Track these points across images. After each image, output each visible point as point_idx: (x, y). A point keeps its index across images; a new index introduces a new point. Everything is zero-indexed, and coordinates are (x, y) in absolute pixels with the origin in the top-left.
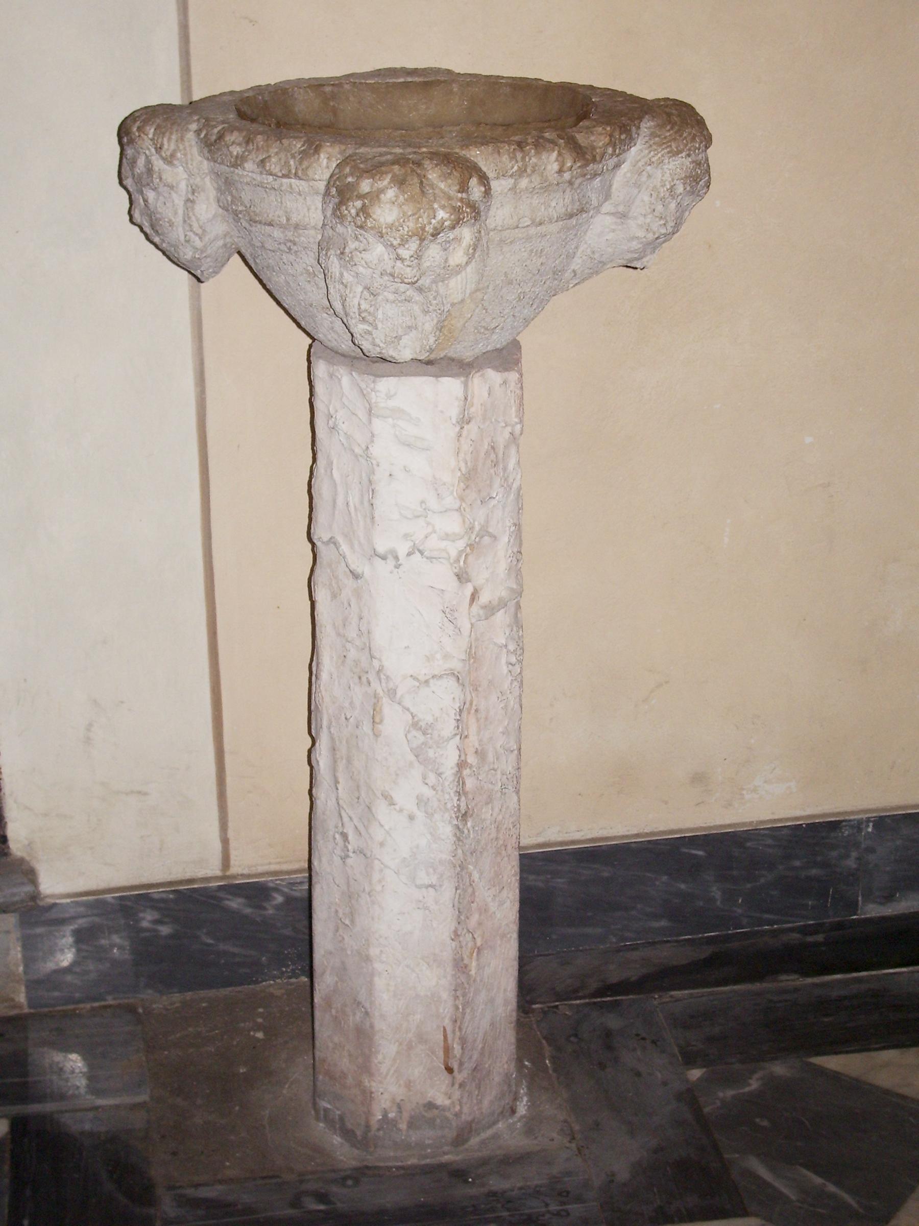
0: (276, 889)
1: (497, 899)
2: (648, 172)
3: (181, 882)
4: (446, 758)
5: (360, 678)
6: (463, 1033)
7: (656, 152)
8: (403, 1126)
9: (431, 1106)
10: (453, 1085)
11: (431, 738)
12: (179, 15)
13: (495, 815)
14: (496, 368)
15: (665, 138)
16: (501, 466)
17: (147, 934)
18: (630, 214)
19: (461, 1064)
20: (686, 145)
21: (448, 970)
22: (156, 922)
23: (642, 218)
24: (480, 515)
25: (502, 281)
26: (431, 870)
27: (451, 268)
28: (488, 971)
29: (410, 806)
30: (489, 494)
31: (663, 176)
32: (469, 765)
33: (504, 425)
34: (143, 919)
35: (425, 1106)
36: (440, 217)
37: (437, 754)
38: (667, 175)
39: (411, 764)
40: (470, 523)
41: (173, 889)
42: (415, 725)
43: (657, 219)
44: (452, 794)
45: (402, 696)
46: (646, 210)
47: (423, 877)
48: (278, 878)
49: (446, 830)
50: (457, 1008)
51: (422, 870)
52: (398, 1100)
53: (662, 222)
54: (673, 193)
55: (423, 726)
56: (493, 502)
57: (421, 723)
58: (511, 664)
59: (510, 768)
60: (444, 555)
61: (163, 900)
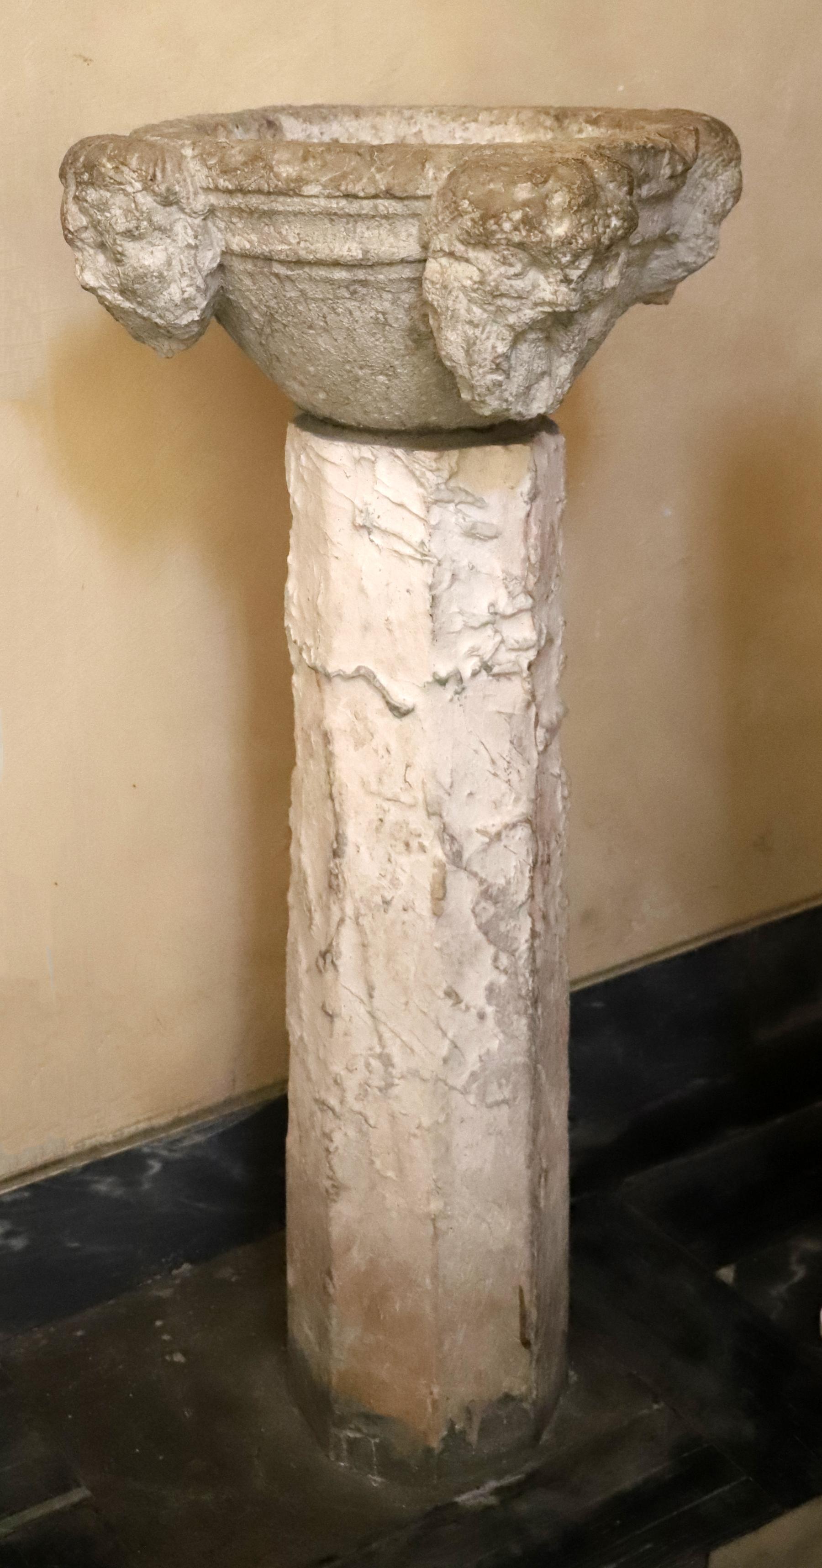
0: (153, 1155)
3: (32, 1171)
8: (473, 1437)
9: (507, 1398)
26: (504, 1081)
38: (721, 188)
41: (28, 1183)
42: (486, 894)
44: (527, 975)
45: (470, 859)
47: (496, 1094)
48: (154, 1138)
55: (494, 893)
60: (516, 669)
61: (14, 1203)
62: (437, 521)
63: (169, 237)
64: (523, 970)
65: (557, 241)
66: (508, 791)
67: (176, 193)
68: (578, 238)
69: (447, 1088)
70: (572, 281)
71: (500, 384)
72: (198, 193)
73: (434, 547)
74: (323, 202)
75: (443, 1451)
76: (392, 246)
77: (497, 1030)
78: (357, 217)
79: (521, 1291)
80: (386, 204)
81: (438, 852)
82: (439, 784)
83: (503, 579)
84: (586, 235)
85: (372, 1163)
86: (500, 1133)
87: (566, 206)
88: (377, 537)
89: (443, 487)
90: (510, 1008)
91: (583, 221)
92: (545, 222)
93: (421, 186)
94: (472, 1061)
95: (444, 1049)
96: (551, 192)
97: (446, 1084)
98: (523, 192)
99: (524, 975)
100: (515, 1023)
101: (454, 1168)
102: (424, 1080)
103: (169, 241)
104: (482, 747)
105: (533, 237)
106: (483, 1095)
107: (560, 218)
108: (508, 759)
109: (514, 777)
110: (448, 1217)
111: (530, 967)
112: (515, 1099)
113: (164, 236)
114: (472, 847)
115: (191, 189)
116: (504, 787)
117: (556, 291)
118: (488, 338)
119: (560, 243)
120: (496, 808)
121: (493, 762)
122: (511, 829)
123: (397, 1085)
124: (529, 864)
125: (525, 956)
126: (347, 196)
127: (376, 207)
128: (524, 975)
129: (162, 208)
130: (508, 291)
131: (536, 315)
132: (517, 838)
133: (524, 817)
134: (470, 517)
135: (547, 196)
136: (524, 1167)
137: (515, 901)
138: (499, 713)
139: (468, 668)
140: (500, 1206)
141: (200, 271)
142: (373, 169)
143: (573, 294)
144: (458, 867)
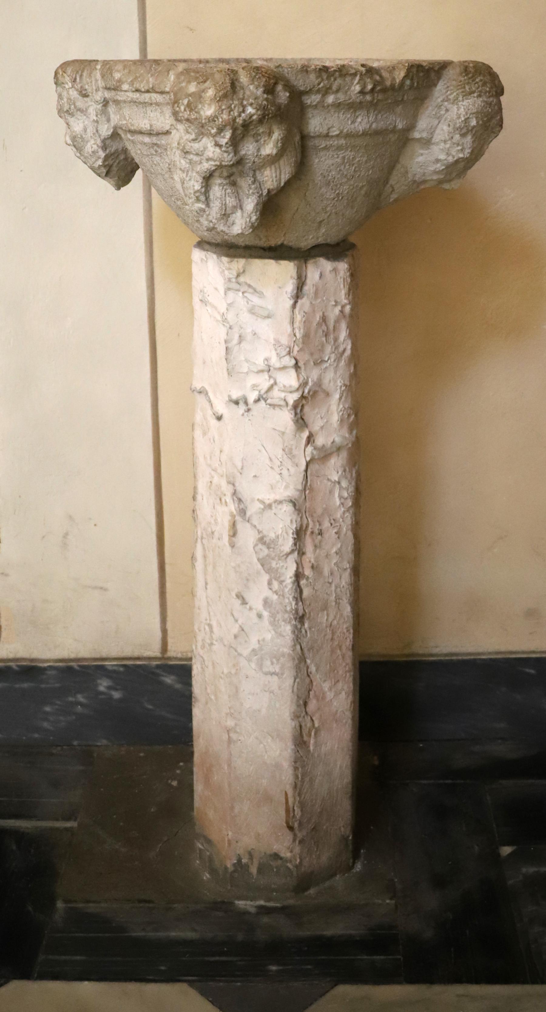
1: (333, 690)
2: (446, 107)
4: (286, 569)
5: (220, 499)
6: (302, 798)
7: (452, 92)
8: (254, 870)
9: (276, 856)
10: (294, 840)
11: (273, 551)
12: (140, 24)
13: (330, 620)
14: (328, 259)
15: (461, 81)
16: (332, 336)
17: (103, 697)
18: (434, 140)
19: (300, 824)
20: (478, 88)
21: (288, 744)
22: (109, 688)
23: (442, 144)
24: (314, 374)
25: (320, 180)
26: (274, 660)
27: (262, 157)
28: (324, 749)
29: (258, 605)
30: (321, 358)
31: (458, 110)
32: (306, 577)
33: (334, 304)
34: (101, 684)
35: (271, 855)
36: (248, 112)
37: (278, 565)
38: (462, 110)
39: (258, 573)
40: (304, 379)
42: (262, 540)
43: (455, 145)
44: (291, 599)
45: (251, 516)
46: (445, 136)
49: (287, 629)
50: (296, 777)
51: (267, 659)
52: (249, 849)
53: (459, 148)
54: (467, 124)
56: (327, 365)
57: (265, 539)
58: (343, 498)
59: (344, 583)
61: (114, 671)
62: (231, 302)
63: (85, 115)
64: (288, 595)
65: (205, 119)
66: (281, 480)
67: (86, 90)
68: (219, 117)
69: (236, 654)
70: (222, 145)
71: (204, 211)
72: (99, 90)
73: (230, 317)
74: (130, 95)
75: (234, 871)
76: (162, 123)
77: (270, 628)
78: (145, 104)
79: (286, 794)
80: (155, 96)
81: (232, 507)
82: (234, 465)
83: (274, 345)
84: (225, 116)
85: (206, 688)
86: (272, 692)
87: (213, 98)
88: (209, 308)
89: (234, 280)
90: (279, 616)
91: (223, 107)
92: (200, 106)
93: (167, 86)
94: (254, 643)
95: (235, 629)
96: (207, 88)
97: (236, 651)
98: (192, 88)
99: (289, 599)
100: (282, 627)
101: (242, 704)
102: (225, 646)
103: (85, 117)
104: (263, 449)
105: (192, 115)
106: (260, 666)
107: (210, 105)
108: (281, 460)
109: (285, 472)
110: (236, 732)
111: (293, 594)
112: (282, 674)
113: (82, 115)
114: (253, 509)
115: (94, 88)
116: (278, 477)
117: (214, 152)
118: (190, 180)
119: (207, 121)
120: (272, 488)
121: (271, 459)
122: (278, 504)
123: (215, 645)
124: (293, 530)
125: (290, 586)
126: (137, 90)
127: (150, 98)
128: (289, 599)
129: (82, 98)
130: (190, 149)
131: (210, 167)
132: (283, 511)
133: (289, 498)
134: (252, 301)
135: (203, 91)
136: (289, 718)
137: (282, 550)
138: (274, 429)
139: (252, 396)
140: (273, 738)
141: (100, 136)
142: (149, 75)
143: (225, 155)
144: (244, 519)
